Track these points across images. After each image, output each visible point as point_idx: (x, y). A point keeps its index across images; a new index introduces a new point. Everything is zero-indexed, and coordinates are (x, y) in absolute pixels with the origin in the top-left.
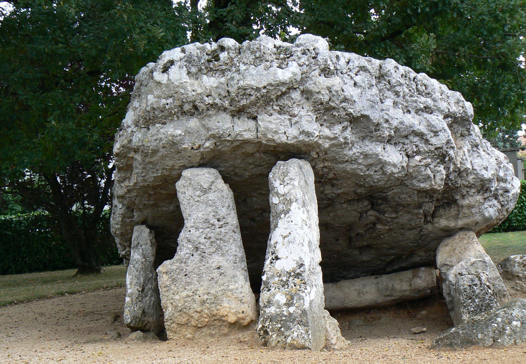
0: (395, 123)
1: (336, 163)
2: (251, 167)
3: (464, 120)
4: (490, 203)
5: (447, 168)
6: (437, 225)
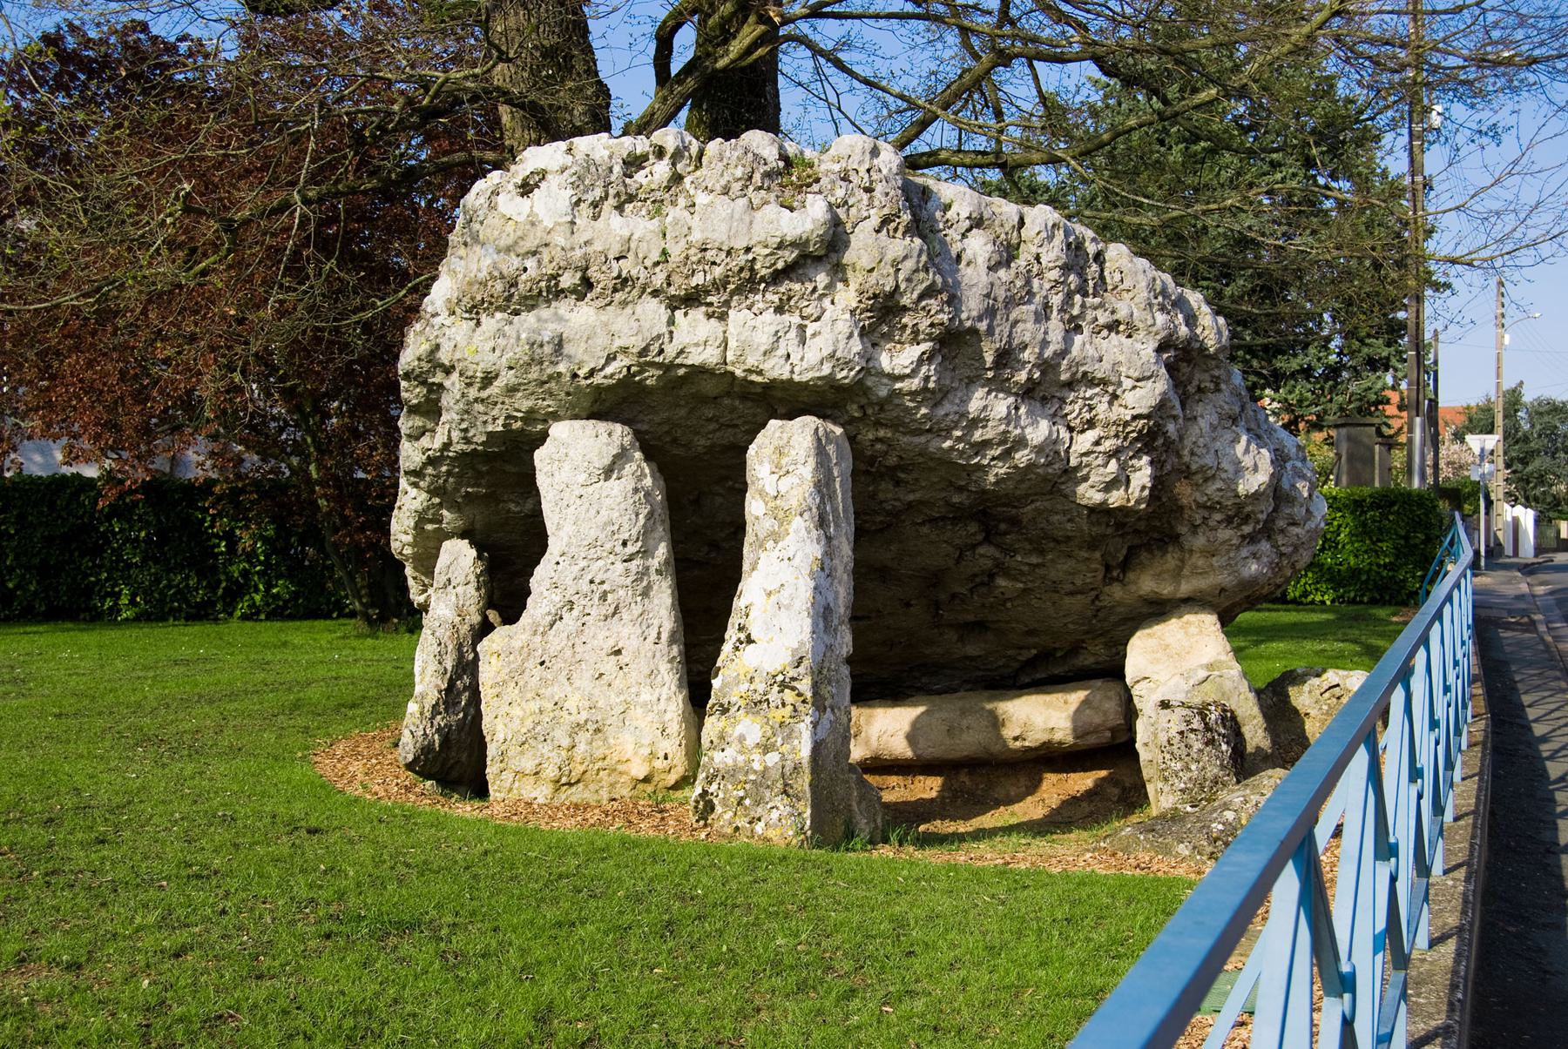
2: (712, 426)
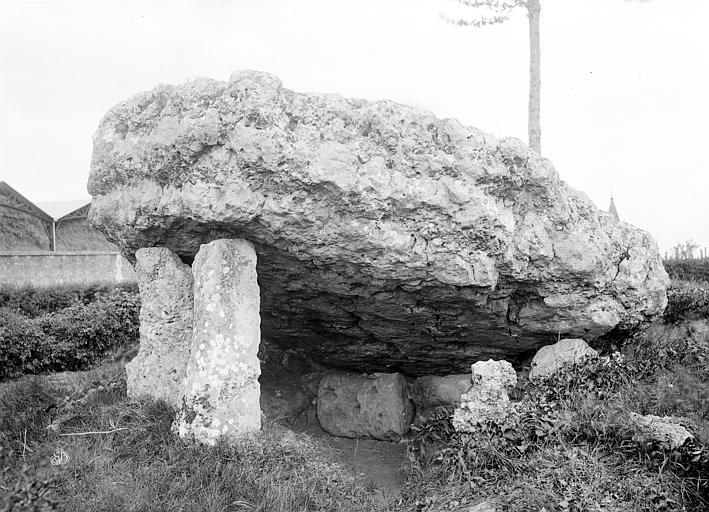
4: (603, 304)
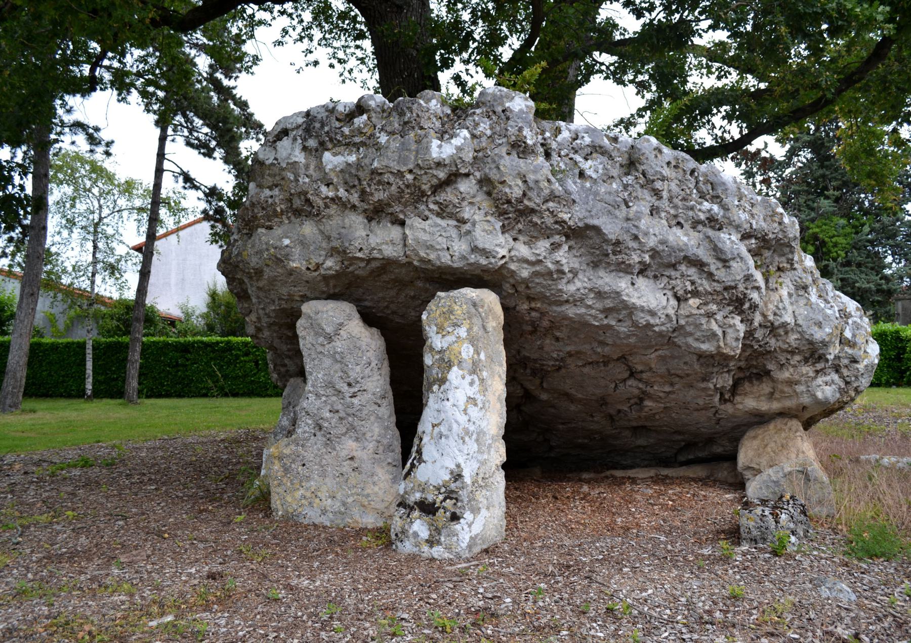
0: (652, 242)
1: (549, 305)
3: (781, 244)
4: (828, 378)
5: (747, 321)
6: (740, 407)
